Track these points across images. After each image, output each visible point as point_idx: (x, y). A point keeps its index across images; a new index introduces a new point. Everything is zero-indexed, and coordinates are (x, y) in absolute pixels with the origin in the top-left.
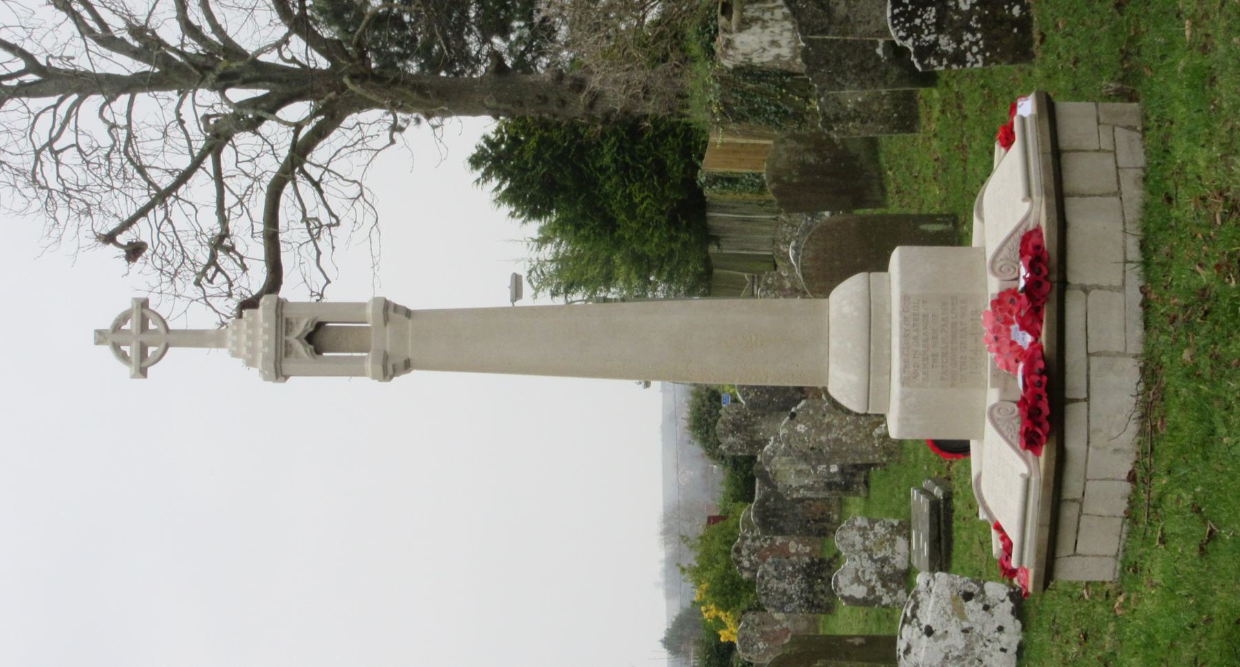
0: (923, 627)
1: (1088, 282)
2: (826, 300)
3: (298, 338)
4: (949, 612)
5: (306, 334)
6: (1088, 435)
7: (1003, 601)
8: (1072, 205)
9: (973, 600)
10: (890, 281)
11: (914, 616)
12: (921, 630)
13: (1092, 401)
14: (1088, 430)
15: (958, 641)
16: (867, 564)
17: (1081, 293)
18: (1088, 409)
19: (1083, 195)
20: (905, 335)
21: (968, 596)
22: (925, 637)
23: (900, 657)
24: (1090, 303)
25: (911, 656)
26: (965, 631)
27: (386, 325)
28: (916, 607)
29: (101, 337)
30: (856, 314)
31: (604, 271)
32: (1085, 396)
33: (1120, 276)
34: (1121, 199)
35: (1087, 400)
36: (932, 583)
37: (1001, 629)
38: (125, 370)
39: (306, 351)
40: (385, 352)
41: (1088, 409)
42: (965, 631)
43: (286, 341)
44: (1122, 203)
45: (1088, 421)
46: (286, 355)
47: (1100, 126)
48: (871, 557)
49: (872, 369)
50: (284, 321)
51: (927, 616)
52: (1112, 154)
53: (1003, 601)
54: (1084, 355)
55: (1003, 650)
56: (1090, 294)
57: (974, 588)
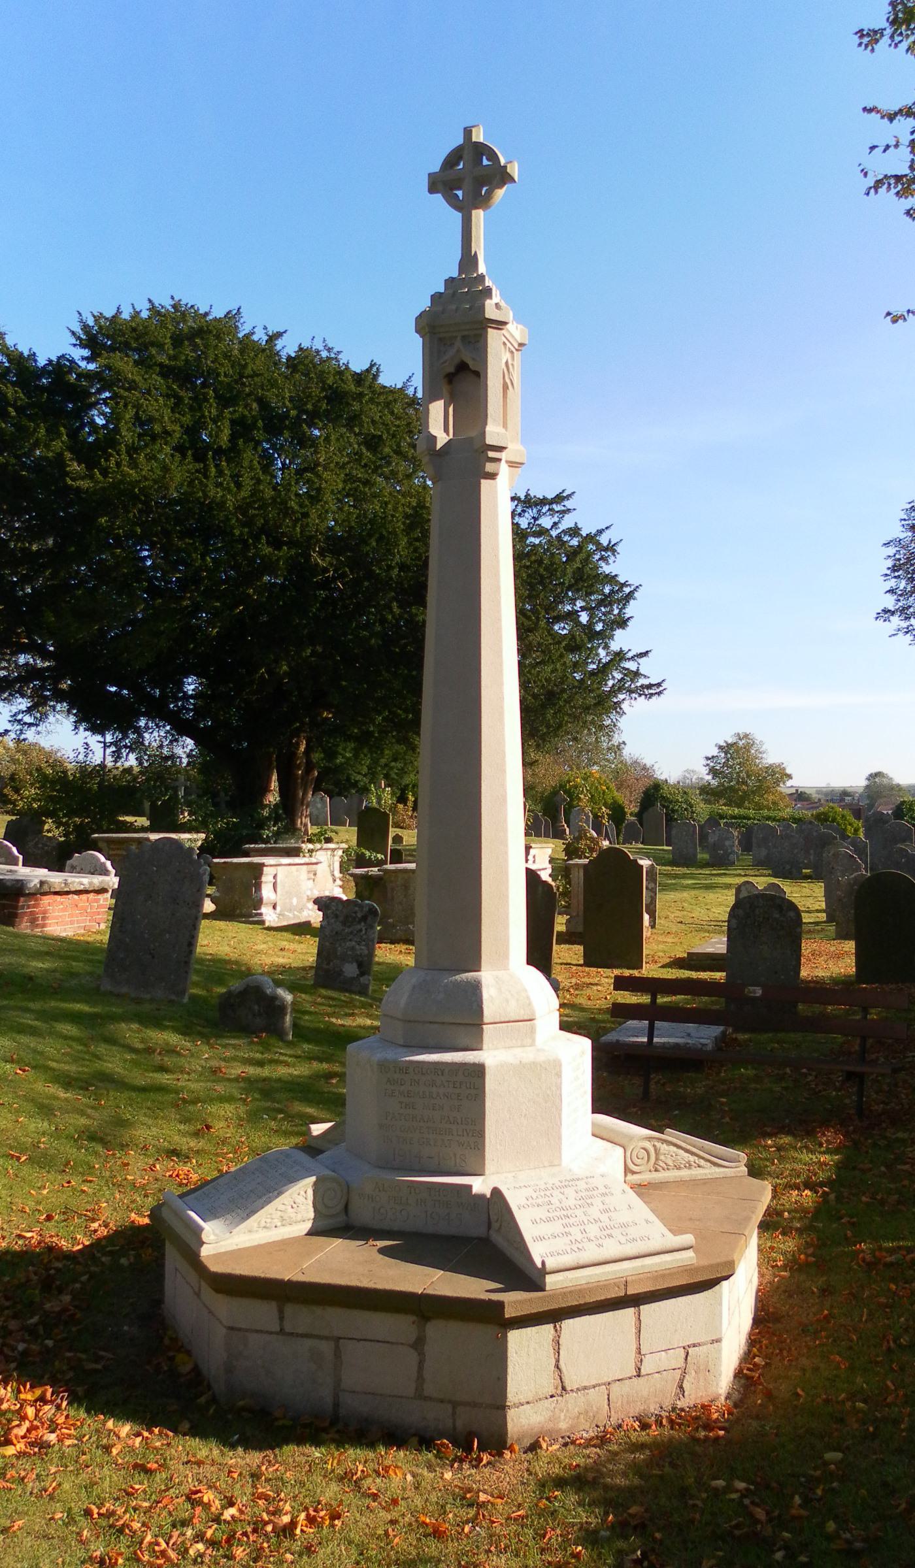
14: (247, 1330)
17: (412, 1337)
18: (271, 1333)
34: (552, 1396)
35: (282, 1331)
41: (271, 1333)
56: (412, 1351)
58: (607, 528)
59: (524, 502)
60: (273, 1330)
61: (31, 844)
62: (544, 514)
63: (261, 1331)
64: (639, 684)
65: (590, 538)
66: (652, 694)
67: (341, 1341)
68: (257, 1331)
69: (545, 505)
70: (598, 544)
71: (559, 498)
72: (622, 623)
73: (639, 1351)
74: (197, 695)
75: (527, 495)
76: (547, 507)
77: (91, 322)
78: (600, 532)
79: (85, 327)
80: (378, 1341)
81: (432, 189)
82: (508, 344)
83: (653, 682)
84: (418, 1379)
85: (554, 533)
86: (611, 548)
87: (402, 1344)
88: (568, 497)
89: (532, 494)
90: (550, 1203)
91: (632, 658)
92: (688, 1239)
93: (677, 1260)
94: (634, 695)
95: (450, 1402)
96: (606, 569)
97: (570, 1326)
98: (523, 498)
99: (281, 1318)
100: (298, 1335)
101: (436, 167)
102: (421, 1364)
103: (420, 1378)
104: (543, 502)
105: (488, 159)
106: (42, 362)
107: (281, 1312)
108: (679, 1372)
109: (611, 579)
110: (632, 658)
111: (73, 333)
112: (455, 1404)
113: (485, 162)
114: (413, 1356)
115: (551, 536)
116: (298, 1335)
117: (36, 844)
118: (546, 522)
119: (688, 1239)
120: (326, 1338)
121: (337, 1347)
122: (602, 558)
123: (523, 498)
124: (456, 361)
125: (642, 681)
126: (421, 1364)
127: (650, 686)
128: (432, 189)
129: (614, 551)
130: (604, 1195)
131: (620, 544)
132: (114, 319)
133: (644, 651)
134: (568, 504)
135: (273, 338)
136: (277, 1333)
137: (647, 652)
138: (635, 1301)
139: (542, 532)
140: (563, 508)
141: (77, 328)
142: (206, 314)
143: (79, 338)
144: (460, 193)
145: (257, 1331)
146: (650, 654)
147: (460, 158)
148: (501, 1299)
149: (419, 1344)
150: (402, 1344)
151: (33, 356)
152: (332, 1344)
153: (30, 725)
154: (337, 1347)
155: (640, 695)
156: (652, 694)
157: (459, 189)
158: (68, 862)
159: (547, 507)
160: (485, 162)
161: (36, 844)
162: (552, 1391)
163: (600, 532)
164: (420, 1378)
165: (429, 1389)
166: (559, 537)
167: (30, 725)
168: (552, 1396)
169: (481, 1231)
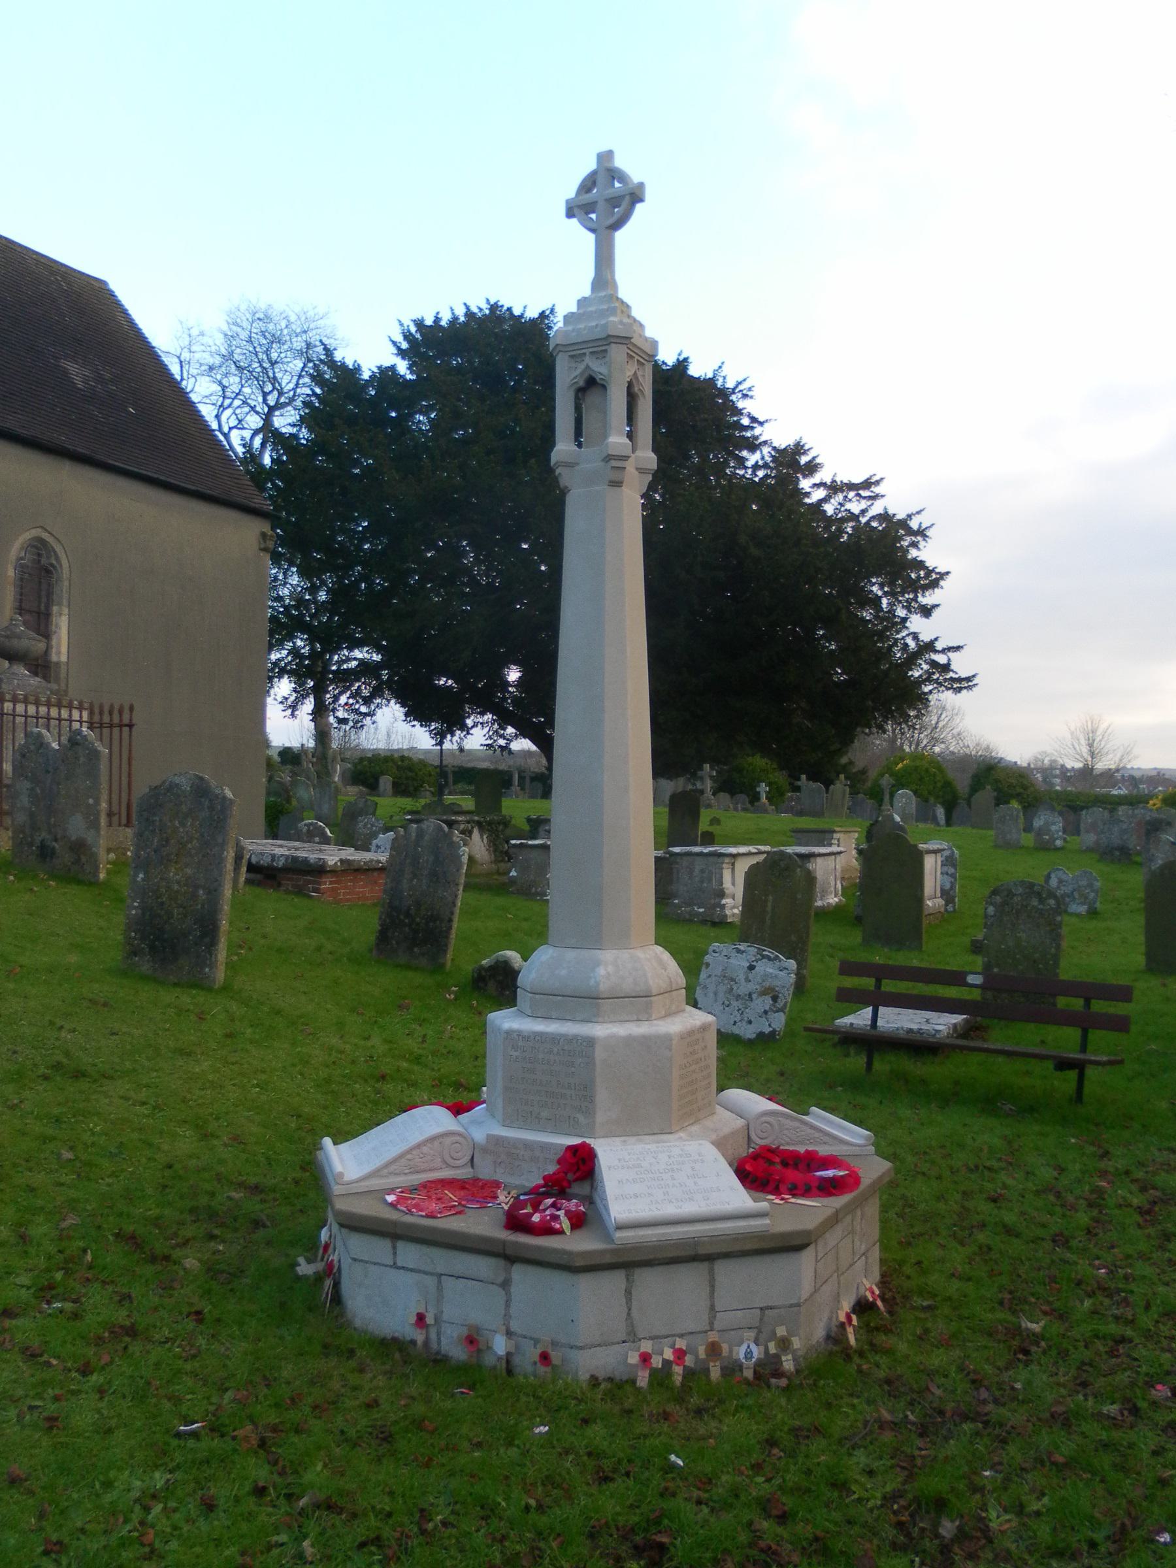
0: (754, 963)
1: (513, 1289)
3: (588, 367)
4: (764, 984)
5: (594, 375)
6: (361, 1261)
7: (770, 1025)
8: (617, 1279)
11: (763, 957)
13: (393, 1271)
14: (367, 1262)
15: (743, 989)
16: (1070, 888)
17: (500, 1279)
18: (386, 1266)
19: (628, 1293)
20: (554, 1039)
21: (775, 999)
25: (734, 954)
26: (750, 995)
27: (603, 460)
28: (769, 959)
29: (605, 158)
30: (592, 982)
32: (399, 1264)
34: (624, 1342)
35: (395, 1266)
37: (750, 1022)
39: (575, 378)
40: (577, 464)
41: (386, 1266)
42: (750, 995)
43: (584, 354)
45: (375, 1264)
46: (572, 357)
47: (758, 1311)
48: (1075, 890)
49: (537, 996)
50: (604, 348)
51: (764, 967)
53: (770, 1025)
54: (439, 1270)
55: (735, 1023)
56: (500, 1289)
57: (780, 1004)
61: (361, 825)
62: (850, 500)
64: (948, 677)
67: (443, 1277)
71: (867, 484)
73: (712, 1308)
74: (520, 683)
78: (910, 516)
79: (407, 336)
81: (570, 214)
82: (637, 357)
83: (963, 676)
86: (921, 533)
88: (877, 483)
89: (838, 480)
90: (640, 1166)
91: (943, 651)
95: (531, 1339)
96: (913, 553)
99: (395, 1254)
101: (571, 193)
104: (851, 486)
105: (619, 182)
106: (366, 375)
107: (394, 1248)
109: (919, 565)
110: (943, 651)
111: (394, 343)
113: (617, 185)
115: (860, 522)
117: (366, 824)
120: (431, 1274)
121: (440, 1282)
124: (586, 375)
127: (960, 680)
128: (570, 214)
129: (925, 536)
130: (695, 1161)
134: (876, 490)
136: (391, 1266)
138: (710, 1258)
139: (853, 517)
140: (872, 494)
141: (399, 338)
142: (521, 316)
143: (399, 349)
144: (593, 216)
147: (594, 184)
148: (509, 1232)
149: (506, 1284)
151: (357, 369)
153: (366, 715)
154: (440, 1282)
155: (948, 689)
157: (593, 212)
158: (374, 842)
160: (617, 185)
161: (366, 824)
162: (623, 1337)
166: (868, 523)
167: (366, 715)
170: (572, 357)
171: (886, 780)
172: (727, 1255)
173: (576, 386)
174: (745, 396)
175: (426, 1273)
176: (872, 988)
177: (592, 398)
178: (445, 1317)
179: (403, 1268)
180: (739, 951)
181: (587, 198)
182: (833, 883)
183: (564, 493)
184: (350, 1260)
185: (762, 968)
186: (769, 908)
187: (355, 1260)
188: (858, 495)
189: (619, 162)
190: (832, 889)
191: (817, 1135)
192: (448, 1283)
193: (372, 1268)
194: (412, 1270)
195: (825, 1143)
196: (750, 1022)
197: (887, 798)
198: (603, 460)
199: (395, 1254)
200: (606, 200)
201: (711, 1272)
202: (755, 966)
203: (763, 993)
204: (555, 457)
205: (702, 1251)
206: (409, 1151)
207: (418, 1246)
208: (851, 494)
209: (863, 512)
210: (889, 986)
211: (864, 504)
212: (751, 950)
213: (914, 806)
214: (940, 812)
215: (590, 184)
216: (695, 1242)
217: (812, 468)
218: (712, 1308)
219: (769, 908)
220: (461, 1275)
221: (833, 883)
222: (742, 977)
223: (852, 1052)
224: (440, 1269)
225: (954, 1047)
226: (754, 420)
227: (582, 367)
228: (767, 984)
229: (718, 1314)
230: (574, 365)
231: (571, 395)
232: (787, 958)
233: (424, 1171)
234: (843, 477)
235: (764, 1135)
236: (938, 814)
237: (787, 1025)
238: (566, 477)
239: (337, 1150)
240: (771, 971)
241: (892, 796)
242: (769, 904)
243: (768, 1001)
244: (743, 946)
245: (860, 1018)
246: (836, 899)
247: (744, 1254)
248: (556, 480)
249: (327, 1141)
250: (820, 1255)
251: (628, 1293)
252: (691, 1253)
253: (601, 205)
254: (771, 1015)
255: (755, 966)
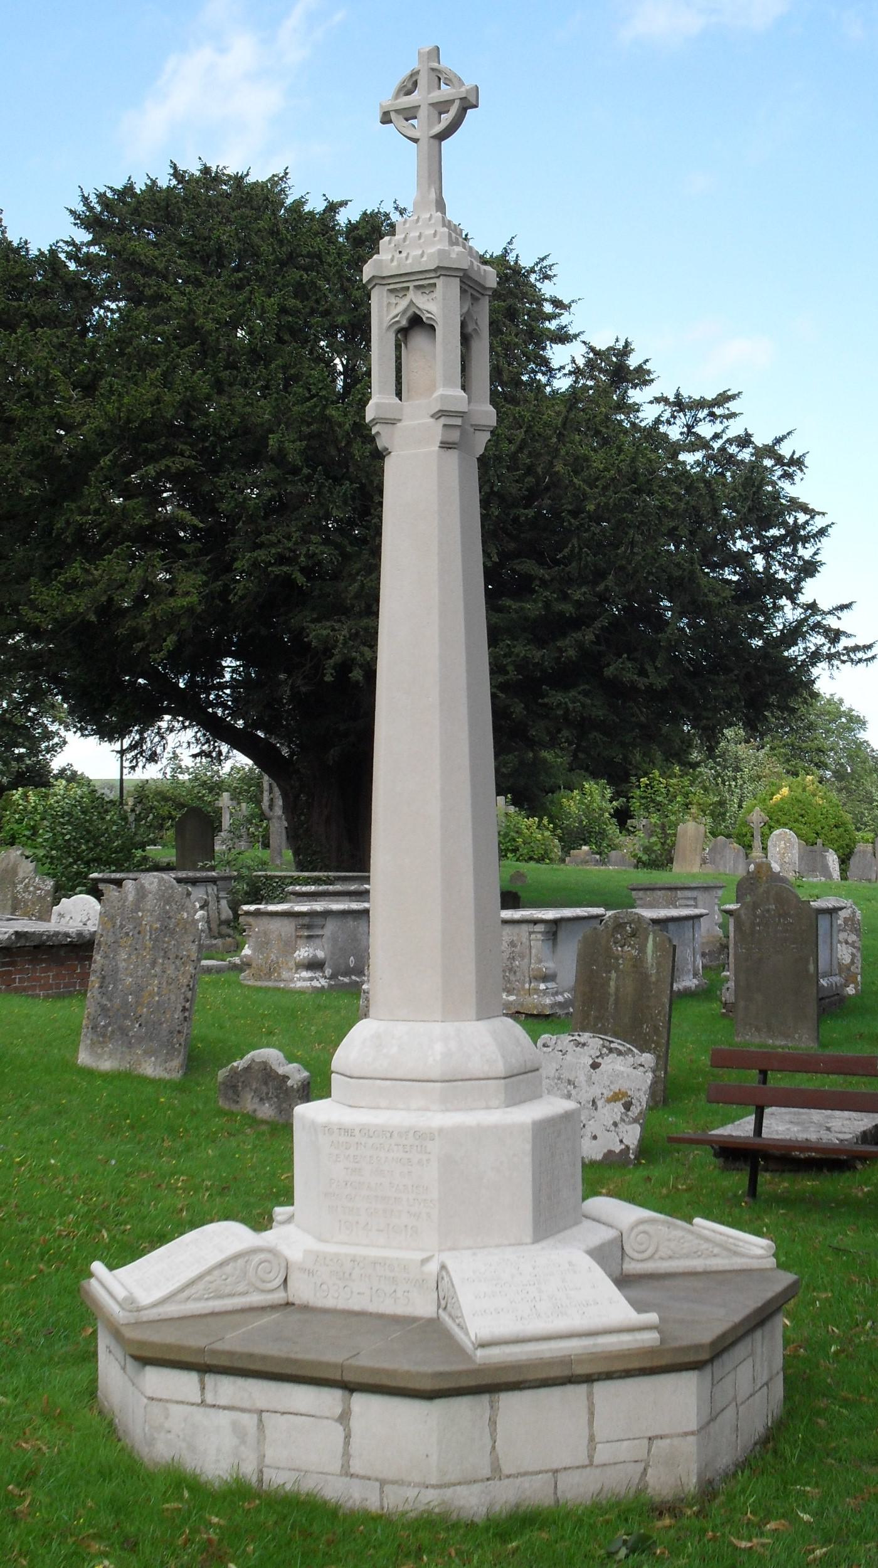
0: (599, 1060)
2: (473, 1012)
5: (419, 313)
7: (621, 1141)
9: (623, 1110)
10: (488, 1108)
11: (611, 1050)
12: (597, 1057)
13: (202, 1409)
14: (167, 1401)
18: (193, 1404)
21: (628, 1106)
22: (591, 1062)
23: (573, 1036)
24: (325, 1422)
25: (571, 1047)
27: (432, 416)
28: (620, 1053)
31: (20, 740)
33: (362, 1472)
34: (488, 1479)
35: (203, 1403)
36: (641, 1069)
38: (386, 97)
40: (400, 420)
41: (193, 1404)
44: (482, 1481)
50: (432, 281)
51: (614, 1065)
52: (587, 1462)
53: (621, 1141)
58: (789, 434)
59: (675, 404)
60: (193, 1401)
63: (182, 1402)
65: (769, 451)
66: (860, 660)
68: (178, 1402)
69: (703, 408)
70: (779, 460)
71: (724, 398)
72: (810, 569)
73: (592, 1438)
75: (678, 395)
76: (706, 412)
77: (93, 199)
78: (779, 441)
80: (301, 1415)
82: (471, 291)
83: (861, 644)
84: (343, 1456)
85: (716, 445)
86: (797, 462)
87: (327, 1418)
89: (685, 394)
92: (652, 1317)
93: (636, 1341)
94: (836, 662)
95: (377, 1480)
97: (508, 1401)
98: (672, 399)
99: (203, 1389)
100: (219, 1407)
102: (348, 1437)
103: (346, 1454)
104: (701, 404)
108: (643, 1465)
112: (383, 1483)
114: (339, 1428)
116: (219, 1407)
118: (705, 430)
119: (652, 1317)
120: (249, 1411)
121: (260, 1420)
122: (787, 476)
123: (672, 399)
124: (409, 314)
125: (844, 642)
126: (348, 1437)
127: (857, 648)
131: (807, 455)
132: (129, 189)
133: (846, 602)
134: (733, 406)
135: (333, 208)
136: (198, 1405)
137: (851, 604)
138: (589, 1379)
140: (727, 412)
145: (178, 1402)
146: (854, 606)
149: (344, 1418)
150: (327, 1418)
152: (255, 1417)
154: (260, 1420)
156: (860, 660)
159: (706, 412)
163: (779, 441)
164: (346, 1454)
165: (356, 1467)
166: (723, 449)
168: (488, 1479)
169: (423, 1307)
170: (391, 291)
171: (757, 816)
172: (609, 1376)
173: (396, 327)
174: (547, 277)
175: (243, 1410)
176: (755, 1084)
177: (418, 340)
178: (267, 1461)
179: (214, 1406)
180: (578, 1044)
181: (406, 101)
182: (690, 959)
183: (379, 456)
184: (145, 1401)
185: (610, 1067)
186: (612, 990)
187: (152, 1399)
188: (712, 414)
189: (446, 62)
190: (690, 967)
191: (705, 1246)
192: (269, 1419)
193: (173, 1408)
194: (225, 1408)
195: (715, 1256)
196: (595, 1138)
197: (757, 843)
198: (432, 416)
199: (203, 1389)
200: (432, 104)
201: (590, 1396)
202: (600, 1064)
203: (615, 1098)
204: (370, 413)
205: (580, 1370)
206: (209, 1272)
207: (231, 1379)
208: (702, 414)
209: (717, 436)
210: (777, 1080)
211: (718, 427)
212: (593, 1042)
213: (795, 851)
214: (832, 860)
215: (410, 86)
216: (566, 1361)
217: (642, 377)
218: (592, 1438)
219: (612, 990)
220: (288, 1410)
221: (690, 959)
222: (582, 1078)
223: (604, 1502)
224: (261, 1404)
225: (864, 1158)
226: (557, 303)
227: (403, 304)
228: (615, 1088)
229: (599, 1446)
230: (393, 300)
231: (391, 337)
232: (642, 1051)
233: (231, 1295)
234: (693, 392)
235: (643, 1247)
236: (830, 864)
237: (642, 1140)
238: (385, 438)
239: (114, 1276)
240: (622, 1069)
241: (765, 838)
242: (612, 983)
243: (618, 1107)
244: (586, 1037)
245: (741, 1128)
246: (695, 981)
247: (627, 1374)
248: (372, 439)
249: (97, 1267)
250: (716, 1378)
251: (493, 1423)
252: (566, 1373)
253: (423, 113)
254: (622, 1127)
255: (600, 1064)
